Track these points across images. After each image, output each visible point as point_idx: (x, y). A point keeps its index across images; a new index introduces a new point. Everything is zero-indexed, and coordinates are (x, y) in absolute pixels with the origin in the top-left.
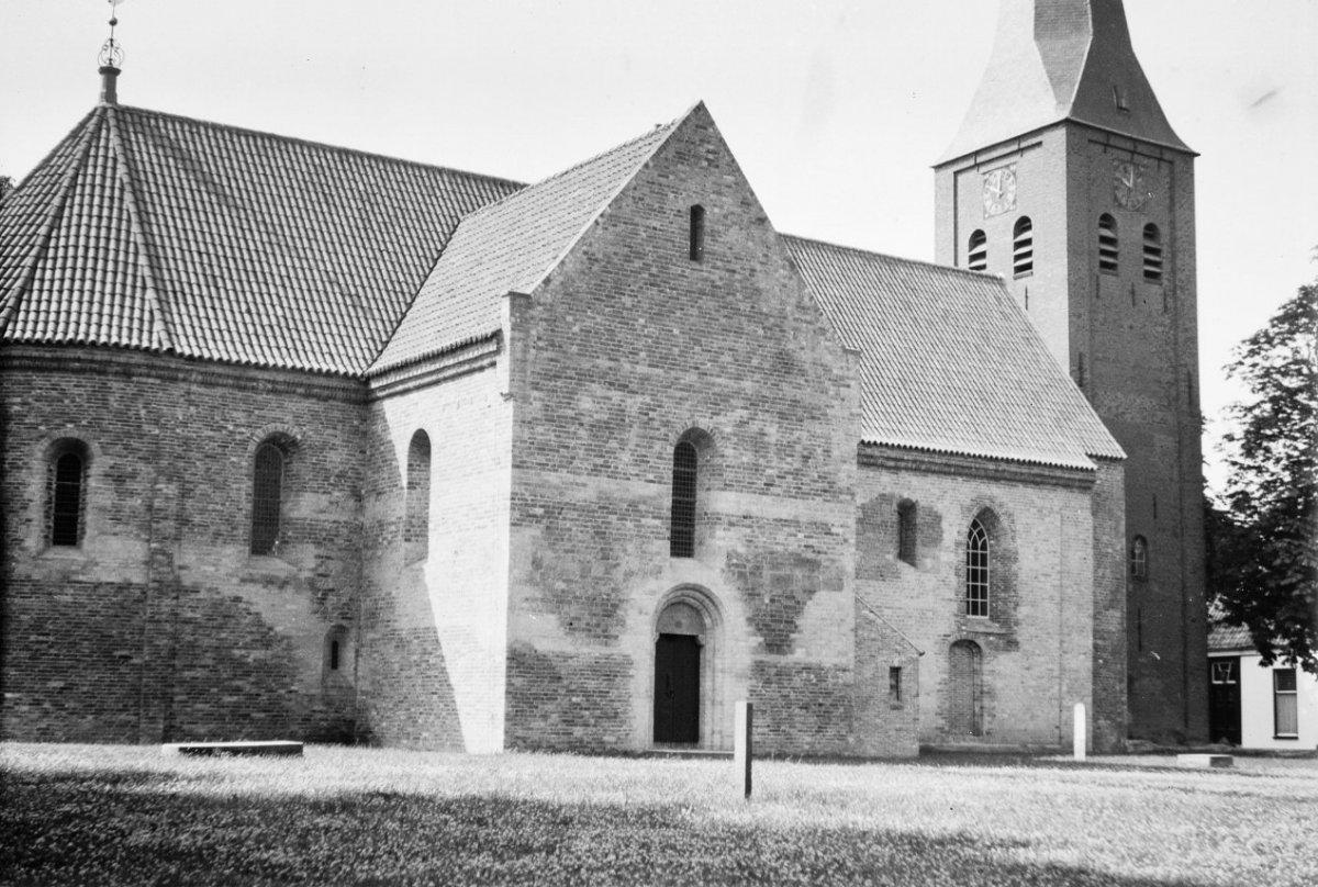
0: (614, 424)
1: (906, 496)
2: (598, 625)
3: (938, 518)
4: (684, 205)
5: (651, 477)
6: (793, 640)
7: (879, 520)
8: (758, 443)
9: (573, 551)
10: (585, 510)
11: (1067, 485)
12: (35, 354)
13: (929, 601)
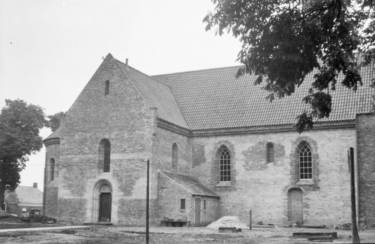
0: (83, 142)
1: (269, 141)
2: (80, 192)
3: (282, 147)
4: (104, 81)
5: (93, 153)
6: (132, 192)
7: (259, 150)
8: (122, 140)
9: (73, 174)
10: (77, 164)
11: (343, 127)
12: (337, 124)
13: (279, 176)
